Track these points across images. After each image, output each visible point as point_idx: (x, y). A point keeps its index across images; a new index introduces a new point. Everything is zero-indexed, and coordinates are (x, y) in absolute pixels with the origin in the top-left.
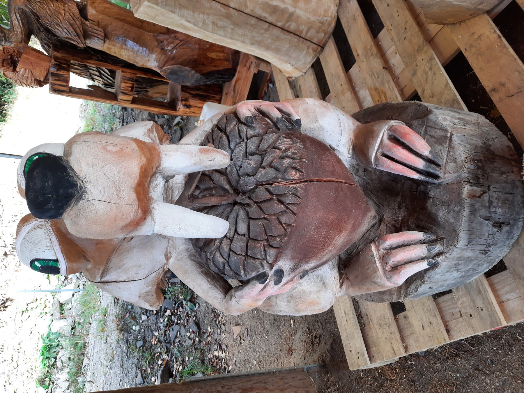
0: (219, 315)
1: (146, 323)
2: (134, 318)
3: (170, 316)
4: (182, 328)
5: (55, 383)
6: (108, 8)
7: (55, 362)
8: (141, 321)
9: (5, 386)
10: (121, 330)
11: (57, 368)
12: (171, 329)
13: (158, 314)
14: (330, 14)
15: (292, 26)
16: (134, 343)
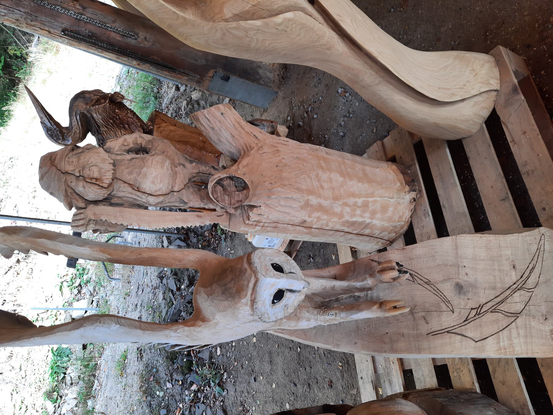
0: (249, 411)
1: (171, 391)
2: (158, 383)
3: (196, 392)
4: (209, 409)
5: (63, 399)
6: (173, 131)
7: (64, 377)
8: (165, 388)
9: (12, 395)
10: (145, 392)
11: (66, 384)
12: (197, 407)
13: (184, 385)
14: (404, 219)
15: (367, 231)
16: (157, 409)
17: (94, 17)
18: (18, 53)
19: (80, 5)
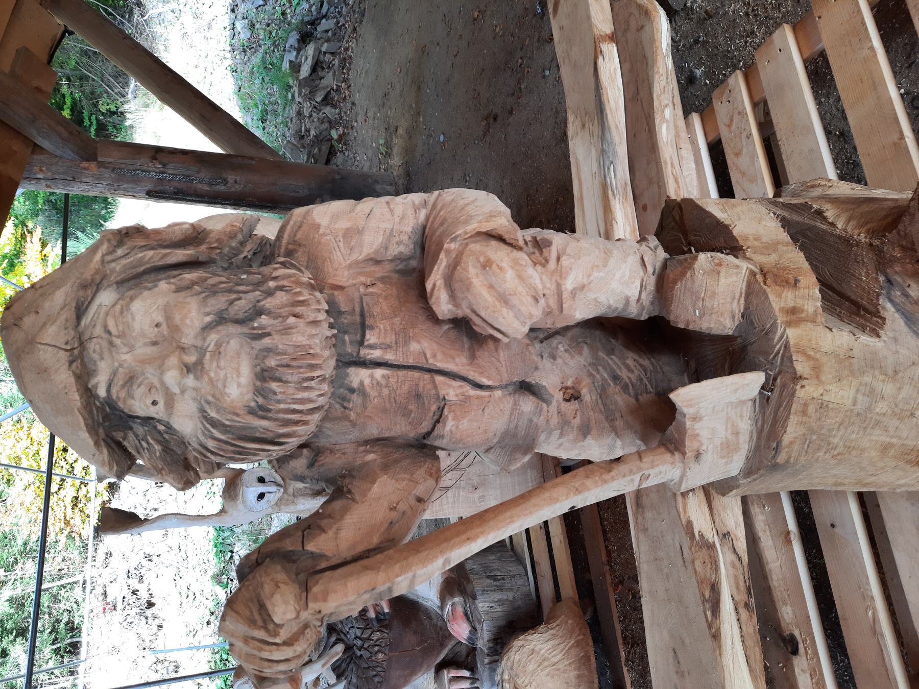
7: (232, 557)
17: (176, 172)
18: (113, 109)
19: (160, 163)
